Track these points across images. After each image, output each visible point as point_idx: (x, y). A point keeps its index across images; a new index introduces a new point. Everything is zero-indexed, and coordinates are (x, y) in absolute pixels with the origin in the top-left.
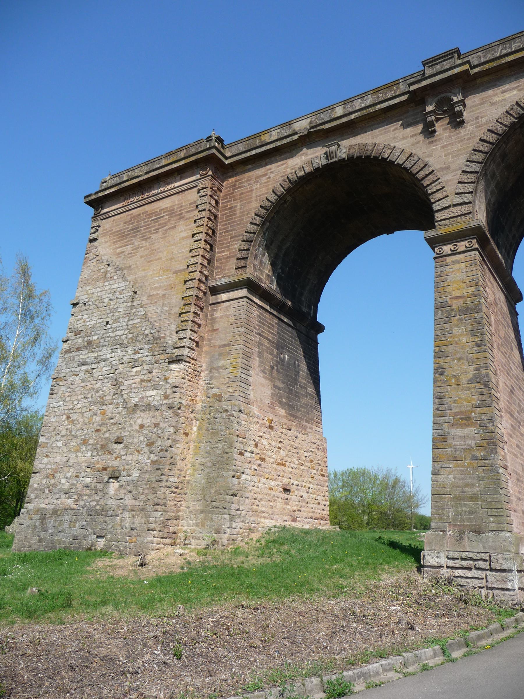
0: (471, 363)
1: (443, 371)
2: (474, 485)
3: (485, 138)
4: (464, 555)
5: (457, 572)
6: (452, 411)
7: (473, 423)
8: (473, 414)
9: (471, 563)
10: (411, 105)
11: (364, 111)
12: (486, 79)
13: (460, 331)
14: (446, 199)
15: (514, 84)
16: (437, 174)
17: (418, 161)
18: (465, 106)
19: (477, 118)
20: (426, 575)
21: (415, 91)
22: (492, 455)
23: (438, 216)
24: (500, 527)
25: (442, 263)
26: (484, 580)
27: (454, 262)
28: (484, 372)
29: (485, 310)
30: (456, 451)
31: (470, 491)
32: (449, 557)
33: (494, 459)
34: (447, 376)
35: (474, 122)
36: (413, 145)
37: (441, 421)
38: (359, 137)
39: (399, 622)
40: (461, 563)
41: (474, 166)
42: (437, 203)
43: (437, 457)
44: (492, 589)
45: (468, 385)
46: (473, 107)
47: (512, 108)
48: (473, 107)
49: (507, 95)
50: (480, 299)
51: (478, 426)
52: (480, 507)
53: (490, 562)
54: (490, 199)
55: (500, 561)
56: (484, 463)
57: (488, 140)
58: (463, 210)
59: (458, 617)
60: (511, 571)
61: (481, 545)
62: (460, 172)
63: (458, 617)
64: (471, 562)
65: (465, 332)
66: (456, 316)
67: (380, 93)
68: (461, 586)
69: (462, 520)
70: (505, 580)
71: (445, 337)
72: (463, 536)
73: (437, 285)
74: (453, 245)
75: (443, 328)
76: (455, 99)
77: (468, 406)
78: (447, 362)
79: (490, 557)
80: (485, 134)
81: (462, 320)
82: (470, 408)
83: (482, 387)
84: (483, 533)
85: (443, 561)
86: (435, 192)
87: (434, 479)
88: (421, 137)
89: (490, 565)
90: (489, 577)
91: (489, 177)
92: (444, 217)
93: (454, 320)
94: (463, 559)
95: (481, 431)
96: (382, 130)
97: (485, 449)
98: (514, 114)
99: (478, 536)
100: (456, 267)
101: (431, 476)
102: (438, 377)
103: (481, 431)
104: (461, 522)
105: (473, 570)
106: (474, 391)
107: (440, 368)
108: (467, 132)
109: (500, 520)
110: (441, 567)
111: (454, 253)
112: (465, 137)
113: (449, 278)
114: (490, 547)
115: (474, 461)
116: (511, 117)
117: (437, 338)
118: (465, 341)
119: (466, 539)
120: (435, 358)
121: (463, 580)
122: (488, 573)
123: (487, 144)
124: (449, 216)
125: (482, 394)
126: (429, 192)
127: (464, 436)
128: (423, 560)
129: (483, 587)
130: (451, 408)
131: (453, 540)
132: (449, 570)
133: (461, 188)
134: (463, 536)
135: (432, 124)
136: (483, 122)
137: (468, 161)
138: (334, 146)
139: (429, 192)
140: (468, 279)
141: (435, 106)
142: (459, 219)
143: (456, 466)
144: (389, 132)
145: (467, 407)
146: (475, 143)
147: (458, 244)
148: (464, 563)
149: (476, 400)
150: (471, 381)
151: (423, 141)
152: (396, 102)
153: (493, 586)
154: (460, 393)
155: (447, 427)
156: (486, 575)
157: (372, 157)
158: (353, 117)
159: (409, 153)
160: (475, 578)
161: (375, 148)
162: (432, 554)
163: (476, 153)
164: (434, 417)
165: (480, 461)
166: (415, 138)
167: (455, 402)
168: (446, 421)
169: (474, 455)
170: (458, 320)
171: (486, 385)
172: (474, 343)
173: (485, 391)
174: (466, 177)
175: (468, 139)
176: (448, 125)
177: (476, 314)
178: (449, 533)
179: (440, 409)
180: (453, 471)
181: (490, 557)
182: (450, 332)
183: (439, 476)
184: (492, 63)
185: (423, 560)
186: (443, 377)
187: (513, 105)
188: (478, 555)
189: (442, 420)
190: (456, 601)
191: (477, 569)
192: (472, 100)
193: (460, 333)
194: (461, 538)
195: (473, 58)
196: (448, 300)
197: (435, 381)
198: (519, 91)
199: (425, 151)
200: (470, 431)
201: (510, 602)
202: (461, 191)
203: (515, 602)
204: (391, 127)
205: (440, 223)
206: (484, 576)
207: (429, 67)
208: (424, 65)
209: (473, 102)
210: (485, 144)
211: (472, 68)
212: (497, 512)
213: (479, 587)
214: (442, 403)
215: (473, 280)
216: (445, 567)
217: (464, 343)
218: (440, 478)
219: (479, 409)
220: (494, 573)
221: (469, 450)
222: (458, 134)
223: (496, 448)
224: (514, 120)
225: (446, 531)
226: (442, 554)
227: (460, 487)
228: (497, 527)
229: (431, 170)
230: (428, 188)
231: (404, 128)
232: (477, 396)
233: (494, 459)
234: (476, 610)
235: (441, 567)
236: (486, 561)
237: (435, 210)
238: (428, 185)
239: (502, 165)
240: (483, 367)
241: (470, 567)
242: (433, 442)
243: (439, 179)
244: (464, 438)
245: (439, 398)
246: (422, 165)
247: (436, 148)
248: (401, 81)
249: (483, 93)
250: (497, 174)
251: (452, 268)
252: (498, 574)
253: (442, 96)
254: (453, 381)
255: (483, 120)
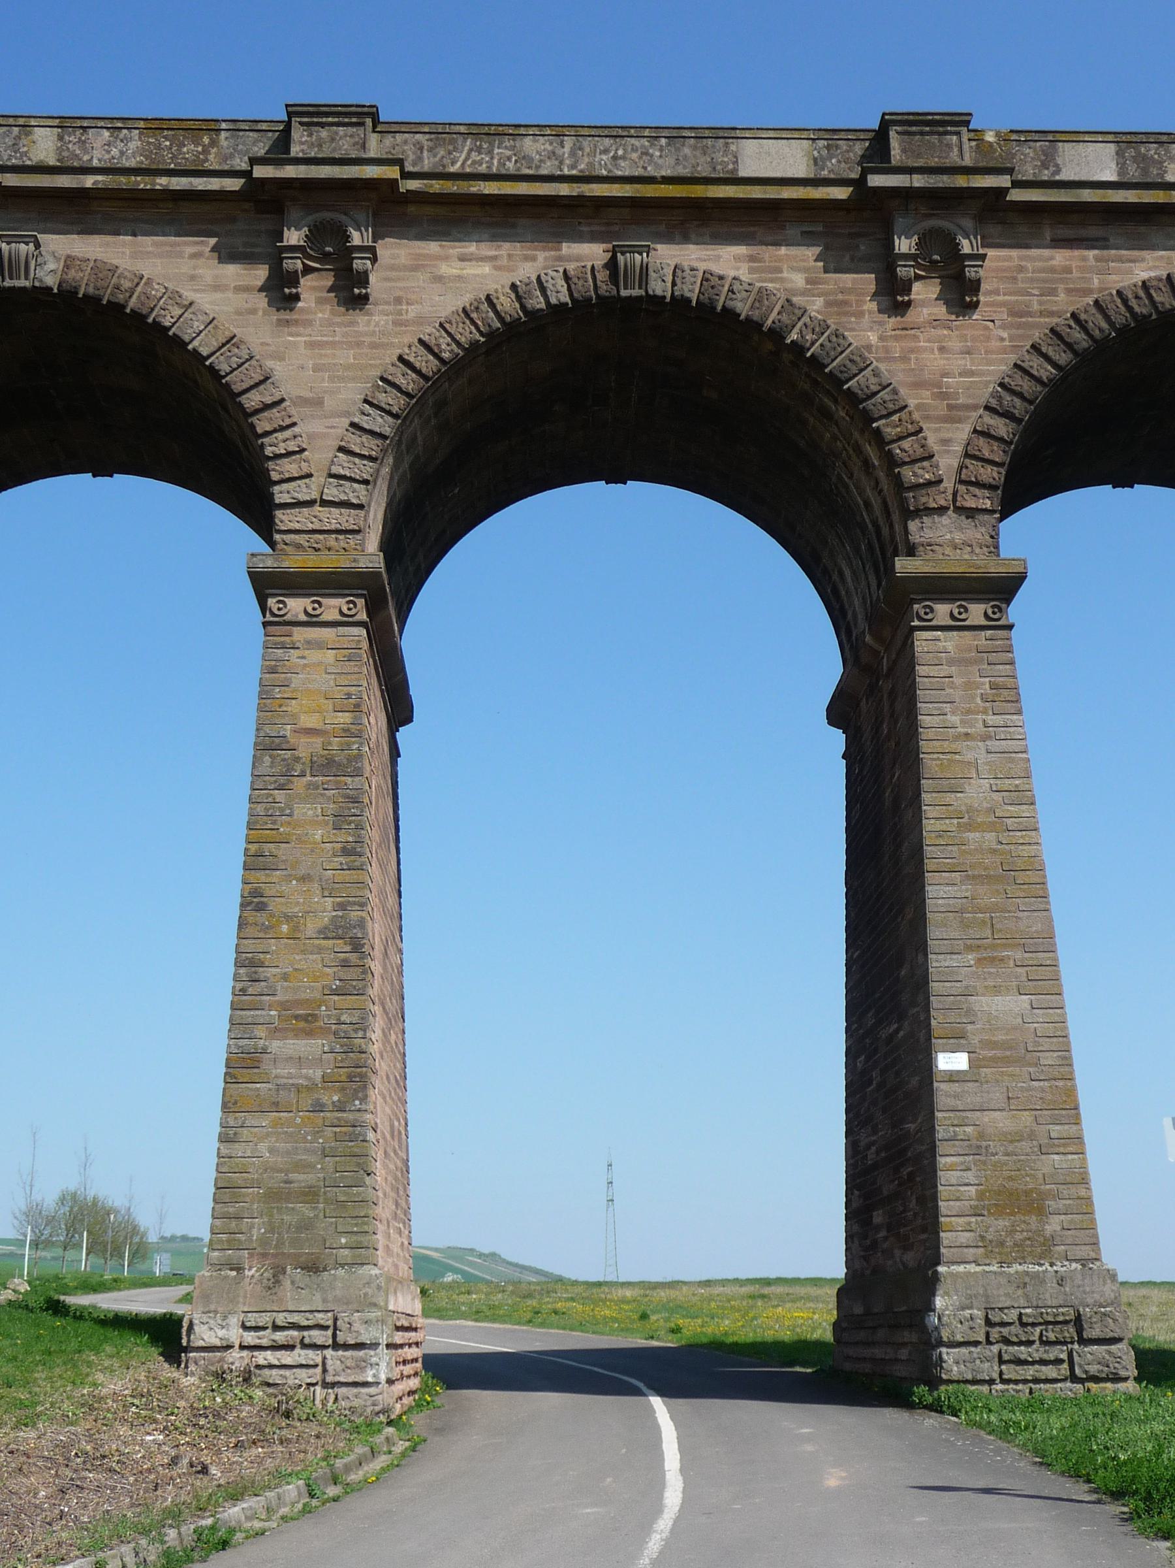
0: (328, 891)
1: (262, 902)
2: (313, 1166)
3: (412, 359)
4: (281, 1319)
5: (262, 1358)
6: (277, 998)
7: (321, 1028)
8: (324, 1008)
9: (296, 1334)
10: (246, 206)
11: (123, 179)
12: (429, 210)
13: (310, 812)
14: (307, 481)
15: (486, 249)
16: (293, 411)
17: (247, 360)
18: (374, 260)
19: (398, 300)
20: (192, 1367)
21: (263, 181)
22: (357, 1102)
23: (284, 518)
24: (360, 1255)
25: (282, 639)
26: (319, 1370)
27: (309, 644)
28: (354, 915)
29: (367, 774)
30: (278, 1090)
31: (301, 1179)
32: (248, 1324)
33: (359, 1110)
34: (272, 916)
35: (391, 308)
36: (238, 313)
37: (250, 1020)
38: (97, 239)
39: (175, 1461)
40: (273, 1337)
41: (380, 420)
42: (285, 486)
43: (235, 1103)
44: (333, 1385)
45: (317, 942)
46: (392, 268)
47: (477, 308)
48: (392, 268)
49: (471, 270)
50: (361, 744)
51: (332, 1037)
52: (321, 1215)
53: (335, 1329)
54: (395, 494)
55: (357, 1326)
56: (338, 1119)
57: (417, 365)
58: (343, 520)
59: (282, 1443)
60: (374, 1346)
61: (318, 1297)
62: (345, 422)
63: (282, 1443)
64: (295, 1333)
65: (321, 818)
66: (303, 775)
67: (166, 138)
68: (269, 1385)
69: (280, 1243)
70: (361, 1365)
71: (274, 823)
72: (281, 1277)
73: (265, 692)
74: (313, 602)
75: (270, 800)
76: (356, 238)
77: (312, 989)
78: (272, 882)
79: (336, 1319)
80: (413, 349)
81: (317, 788)
82: (317, 995)
83: (348, 948)
84: (325, 1270)
85: (234, 1334)
86: (281, 456)
87: (224, 1152)
88: (261, 301)
89: (334, 1336)
90: (329, 1362)
91: (403, 447)
92: (297, 526)
93: (299, 784)
94: (276, 1328)
95: (338, 1048)
96: (165, 244)
97: (343, 1089)
98: (480, 323)
99: (314, 1277)
100: (314, 656)
101: (217, 1145)
102: (251, 916)
103: (338, 1048)
104: (276, 1247)
105: (298, 1351)
106: (329, 957)
107: (256, 893)
108: (371, 328)
109: (361, 1242)
110: (229, 1347)
111: (312, 622)
112: (367, 339)
113: (296, 681)
114: (336, 1300)
115: (316, 1114)
116: (473, 328)
117: (256, 822)
118: (318, 838)
119: (287, 1283)
120: (246, 868)
121: (274, 1372)
122: (329, 1353)
123: (414, 375)
124: (310, 526)
125: (345, 964)
126: (269, 451)
127: (298, 1057)
128: (188, 1336)
129: (316, 1384)
130: (276, 990)
131: (259, 1288)
132: (245, 1353)
133: (344, 464)
134: (281, 1277)
135: (293, 279)
136: (411, 315)
137: (366, 401)
138: (27, 243)
139: (269, 451)
140: (339, 693)
141: (306, 236)
142: (331, 540)
143: (275, 1124)
144: (180, 255)
145: (309, 990)
146: (388, 361)
147: (325, 601)
148: (280, 1337)
149: (331, 976)
150: (324, 934)
151: (265, 313)
152: (209, 187)
153: (337, 1379)
154: (297, 958)
155: (263, 1035)
156: (324, 1358)
157: (128, 311)
158: (89, 181)
159: (228, 334)
160: (301, 1366)
161: (139, 289)
162: (212, 1322)
163: (389, 389)
164: (233, 1008)
165: (328, 1114)
166: (245, 295)
167: (285, 977)
168: (262, 1021)
169: (318, 1099)
170: (309, 786)
171: (357, 946)
172: (340, 845)
173: (353, 957)
174: (358, 440)
175: (373, 346)
176: (329, 291)
177: (350, 779)
178: (250, 1273)
179: (250, 991)
180: (268, 1135)
181: (336, 1319)
182: (288, 812)
183: (237, 1146)
184: (449, 183)
185: (188, 1336)
186: (261, 917)
187: (479, 301)
188: (310, 1316)
189: (253, 1016)
190: (268, 1415)
191: (305, 1346)
192: (394, 252)
193: (309, 815)
194: (277, 1282)
195: (406, 142)
196: (288, 734)
197: (242, 924)
198: (497, 268)
199: (269, 341)
200: (315, 1046)
201: (369, 1410)
202: (342, 472)
203: (377, 1409)
204: (186, 244)
205: (288, 538)
206: (319, 1360)
207: (301, 123)
208: (290, 114)
209: (393, 257)
210: (409, 372)
211: (406, 175)
212: (356, 1225)
213: (308, 1384)
214: (256, 977)
215: (349, 696)
216: (237, 1346)
217: (315, 843)
218: (238, 1149)
219: (336, 998)
220: (340, 1353)
221: (308, 1088)
222: (352, 323)
223: (365, 1087)
224: (478, 337)
225: (244, 1269)
226: (234, 1321)
227: (281, 1171)
228: (354, 1256)
229: (277, 398)
230: (266, 440)
231: (221, 260)
232: (335, 969)
233: (359, 1110)
234: (313, 1429)
235: (229, 1347)
236: (326, 1328)
237: (277, 501)
238: (267, 434)
239: (433, 422)
240: (354, 903)
241: (291, 1343)
242: (227, 1066)
243: (294, 424)
244: (300, 1061)
245: (249, 966)
246: (258, 377)
247: (294, 342)
248: (224, 126)
249: (419, 243)
250: (420, 440)
251: (303, 657)
252: (349, 1353)
253: (327, 215)
254: (285, 928)
255: (412, 312)
